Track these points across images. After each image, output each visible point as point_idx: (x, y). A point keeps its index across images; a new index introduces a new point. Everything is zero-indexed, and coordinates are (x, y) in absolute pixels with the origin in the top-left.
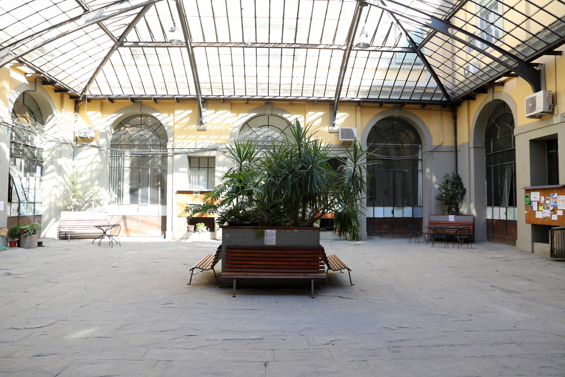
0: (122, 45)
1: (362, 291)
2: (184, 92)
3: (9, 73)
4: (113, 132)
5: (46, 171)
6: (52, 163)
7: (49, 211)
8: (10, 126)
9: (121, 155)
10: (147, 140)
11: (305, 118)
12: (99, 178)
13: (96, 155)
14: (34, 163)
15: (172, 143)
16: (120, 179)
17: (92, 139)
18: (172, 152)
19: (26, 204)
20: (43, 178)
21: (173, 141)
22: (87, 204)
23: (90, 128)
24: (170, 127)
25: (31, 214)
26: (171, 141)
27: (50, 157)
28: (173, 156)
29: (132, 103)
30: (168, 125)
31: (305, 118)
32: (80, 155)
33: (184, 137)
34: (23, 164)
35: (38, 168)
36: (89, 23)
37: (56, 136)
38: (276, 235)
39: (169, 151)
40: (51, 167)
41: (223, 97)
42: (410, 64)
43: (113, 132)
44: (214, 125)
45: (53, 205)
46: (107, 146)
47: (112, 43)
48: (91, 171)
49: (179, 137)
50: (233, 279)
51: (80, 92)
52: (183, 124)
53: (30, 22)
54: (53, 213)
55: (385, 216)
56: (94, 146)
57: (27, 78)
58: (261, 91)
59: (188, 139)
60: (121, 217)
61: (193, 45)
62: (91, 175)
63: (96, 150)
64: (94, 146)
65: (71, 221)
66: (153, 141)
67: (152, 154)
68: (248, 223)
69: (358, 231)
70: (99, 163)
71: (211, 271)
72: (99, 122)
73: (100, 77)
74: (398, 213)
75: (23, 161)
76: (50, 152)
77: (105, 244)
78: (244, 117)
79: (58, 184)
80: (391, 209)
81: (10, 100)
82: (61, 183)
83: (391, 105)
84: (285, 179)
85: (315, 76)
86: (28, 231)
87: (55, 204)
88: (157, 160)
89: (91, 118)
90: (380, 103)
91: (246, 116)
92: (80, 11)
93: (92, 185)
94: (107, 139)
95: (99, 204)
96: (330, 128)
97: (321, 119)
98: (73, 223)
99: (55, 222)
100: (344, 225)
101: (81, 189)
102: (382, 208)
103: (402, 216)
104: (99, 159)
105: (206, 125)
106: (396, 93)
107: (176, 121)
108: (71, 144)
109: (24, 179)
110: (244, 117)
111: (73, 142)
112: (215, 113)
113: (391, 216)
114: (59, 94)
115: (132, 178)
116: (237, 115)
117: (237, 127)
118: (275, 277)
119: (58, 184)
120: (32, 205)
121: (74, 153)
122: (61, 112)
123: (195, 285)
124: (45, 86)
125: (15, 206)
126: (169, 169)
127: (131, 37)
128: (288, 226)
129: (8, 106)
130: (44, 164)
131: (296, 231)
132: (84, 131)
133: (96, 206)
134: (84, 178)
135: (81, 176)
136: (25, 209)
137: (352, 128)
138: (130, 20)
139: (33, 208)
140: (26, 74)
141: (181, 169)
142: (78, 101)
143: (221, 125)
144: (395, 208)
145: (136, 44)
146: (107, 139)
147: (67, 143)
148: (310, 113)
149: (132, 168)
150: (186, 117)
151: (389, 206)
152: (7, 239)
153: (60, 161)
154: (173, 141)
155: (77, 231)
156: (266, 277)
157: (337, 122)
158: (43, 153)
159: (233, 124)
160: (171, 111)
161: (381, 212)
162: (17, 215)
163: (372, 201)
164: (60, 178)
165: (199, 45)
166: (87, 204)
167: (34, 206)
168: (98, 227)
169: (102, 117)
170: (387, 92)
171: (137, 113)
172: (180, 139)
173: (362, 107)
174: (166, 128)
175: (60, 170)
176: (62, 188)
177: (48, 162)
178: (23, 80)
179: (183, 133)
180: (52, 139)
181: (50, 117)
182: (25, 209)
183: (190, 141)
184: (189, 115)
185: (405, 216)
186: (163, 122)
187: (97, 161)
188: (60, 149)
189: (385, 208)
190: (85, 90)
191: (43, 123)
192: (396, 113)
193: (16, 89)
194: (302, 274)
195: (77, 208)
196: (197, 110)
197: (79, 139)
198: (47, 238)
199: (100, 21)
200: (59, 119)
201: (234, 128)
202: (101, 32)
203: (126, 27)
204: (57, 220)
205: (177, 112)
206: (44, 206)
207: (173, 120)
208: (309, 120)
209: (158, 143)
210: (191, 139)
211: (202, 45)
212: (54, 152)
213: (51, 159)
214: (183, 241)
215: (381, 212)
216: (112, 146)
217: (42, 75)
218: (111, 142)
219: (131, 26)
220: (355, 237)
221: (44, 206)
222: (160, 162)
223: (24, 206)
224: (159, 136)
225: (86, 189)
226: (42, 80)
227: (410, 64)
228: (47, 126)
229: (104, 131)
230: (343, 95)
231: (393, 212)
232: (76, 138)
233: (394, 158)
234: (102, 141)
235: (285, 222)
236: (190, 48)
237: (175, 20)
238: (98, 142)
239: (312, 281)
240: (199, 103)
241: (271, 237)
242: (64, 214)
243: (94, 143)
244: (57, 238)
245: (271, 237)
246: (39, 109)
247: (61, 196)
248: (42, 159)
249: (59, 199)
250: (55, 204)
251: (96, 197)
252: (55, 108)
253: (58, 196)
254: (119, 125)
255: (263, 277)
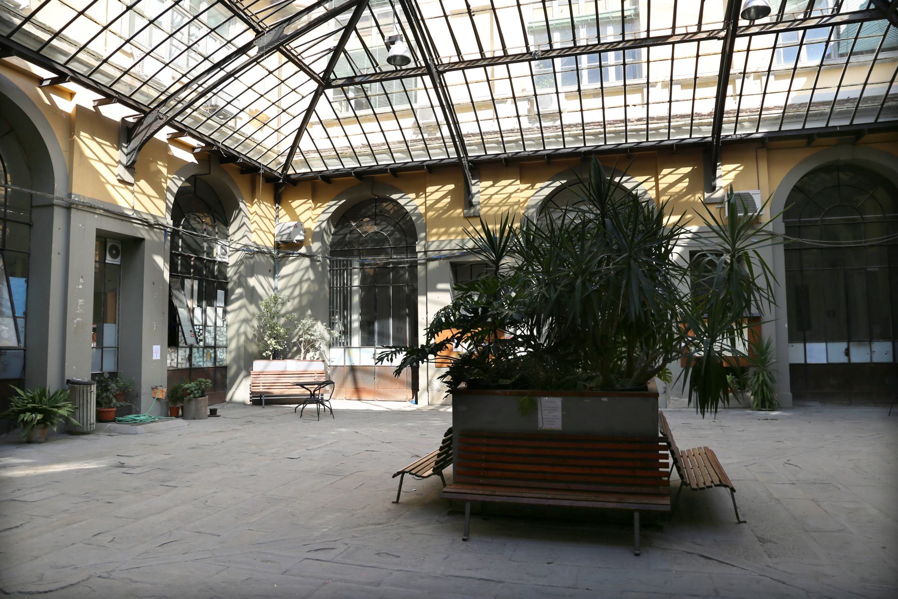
0: (329, 86)
1: (762, 540)
2: (438, 155)
3: (168, 149)
4: (333, 230)
5: (233, 297)
6: (239, 284)
7: (236, 359)
8: (168, 230)
9: (347, 266)
10: (385, 240)
11: (657, 181)
12: (311, 305)
13: (307, 269)
14: (212, 285)
15: (423, 243)
16: (346, 306)
17: (300, 244)
18: (424, 257)
19: (201, 349)
20: (229, 308)
21: (425, 238)
22: (295, 348)
23: (296, 226)
24: (420, 216)
25: (210, 364)
26: (422, 240)
27: (237, 275)
28: (425, 264)
29: (358, 181)
30: (417, 211)
31: (657, 181)
32: (286, 270)
33: (442, 230)
34: (196, 287)
35: (220, 293)
36: (266, 52)
37: (245, 241)
38: (563, 410)
39: (419, 255)
40: (239, 291)
41: (505, 155)
42: (872, 51)
43: (333, 230)
44: (492, 207)
45: (242, 350)
46: (323, 253)
47: (314, 85)
48: (300, 295)
49: (434, 231)
50: (465, 501)
51: (280, 171)
52: (441, 208)
53: (183, 64)
54: (242, 363)
55: (831, 361)
56: (303, 255)
57: (195, 155)
58: (571, 139)
59: (450, 234)
60: (347, 370)
61: (441, 69)
62: (300, 301)
63: (307, 262)
64: (303, 255)
65: (270, 373)
66: (396, 240)
67: (393, 263)
68: (508, 382)
69: (771, 391)
70: (312, 281)
71: (436, 477)
72: (311, 215)
73: (305, 143)
74: (860, 355)
75: (196, 283)
76: (236, 268)
77: (310, 412)
78: (544, 189)
79: (250, 317)
80: (843, 346)
81: (169, 189)
82: (253, 315)
83: (832, 140)
84: (571, 288)
85: (669, 95)
86: (192, 392)
87: (246, 349)
88: (402, 272)
89: (298, 211)
90: (807, 138)
91: (547, 186)
92: (250, 35)
93: (302, 316)
94: (323, 242)
95: (313, 346)
96: (707, 195)
97: (687, 180)
98: (271, 379)
99: (245, 377)
100: (712, 386)
101: (284, 326)
102: (823, 345)
103: (868, 361)
104: (311, 275)
105: (478, 207)
106: (842, 114)
107: (429, 203)
108: (270, 253)
109: (198, 312)
110: (544, 189)
111: (273, 251)
112: (493, 186)
113: (844, 360)
114: (248, 176)
115: (363, 303)
116: (533, 186)
117: (533, 207)
118: (552, 502)
119: (250, 317)
120: (212, 351)
121: (275, 267)
122: (252, 205)
123: (408, 504)
124: (225, 166)
125: (183, 353)
126: (420, 285)
127: (342, 70)
128: (591, 388)
129: (165, 199)
130: (230, 286)
131: (605, 399)
132: (288, 231)
133: (307, 351)
134: (289, 306)
135: (283, 304)
136: (200, 357)
137: (751, 192)
138: (333, 42)
139: (213, 355)
140: (193, 148)
141: (440, 286)
142: (281, 186)
143: (504, 205)
144: (851, 344)
145: (350, 81)
146: (323, 242)
147: (263, 253)
148: (665, 171)
149: (362, 286)
150: (444, 197)
151: (840, 340)
152: (167, 403)
153: (252, 281)
154: (425, 238)
155: (276, 391)
156: (533, 501)
157: (719, 183)
158: (228, 269)
159: (525, 201)
160: (420, 189)
161: (818, 353)
162: (188, 366)
163: (802, 329)
164: (253, 308)
165: (452, 67)
166: (295, 348)
167: (215, 352)
168: (302, 385)
169: (315, 208)
170: (821, 114)
171: (366, 195)
172: (436, 234)
173: (769, 149)
174: (414, 218)
175: (252, 295)
176: (255, 323)
177: (235, 283)
178: (189, 158)
179: (441, 225)
180: (238, 246)
181: (235, 213)
182: (200, 357)
183: (453, 237)
184: (450, 192)
185: (875, 360)
186: (408, 208)
187: (309, 279)
188: (252, 261)
189: (830, 345)
190: (286, 166)
191: (227, 224)
192: (844, 155)
193: (179, 173)
194: (613, 498)
195: (276, 355)
196: (462, 184)
197: (282, 245)
198: (235, 403)
199: (282, 44)
200: (249, 215)
201: (528, 208)
202: (291, 68)
203: (331, 55)
204: (249, 374)
205: (429, 189)
206: (230, 352)
207: (426, 201)
208: (663, 183)
209: (404, 244)
210: (454, 233)
211: (456, 67)
212: (242, 267)
213: (239, 278)
214: (442, 410)
215: (818, 353)
216: (333, 253)
217: (215, 148)
218: (331, 246)
219: (338, 50)
220: (766, 403)
221: (230, 352)
222: (407, 275)
223: (198, 352)
224: (402, 231)
225: (291, 325)
226: (215, 157)
227: (872, 51)
228: (232, 229)
229: (318, 229)
230: (727, 131)
231: (847, 353)
232: (278, 244)
233: (847, 242)
234: (316, 246)
235: (586, 380)
236: (436, 75)
237: (572, 123)
238: (309, 248)
239: (637, 516)
240: (463, 170)
241: (551, 413)
242: (258, 365)
243: (303, 250)
244: (249, 403)
245: (551, 413)
246: (220, 202)
247: (254, 335)
248: (226, 278)
249: (252, 340)
250: (246, 349)
251: (307, 337)
252: (243, 199)
253: (250, 336)
254: (339, 219)
255: (525, 501)
